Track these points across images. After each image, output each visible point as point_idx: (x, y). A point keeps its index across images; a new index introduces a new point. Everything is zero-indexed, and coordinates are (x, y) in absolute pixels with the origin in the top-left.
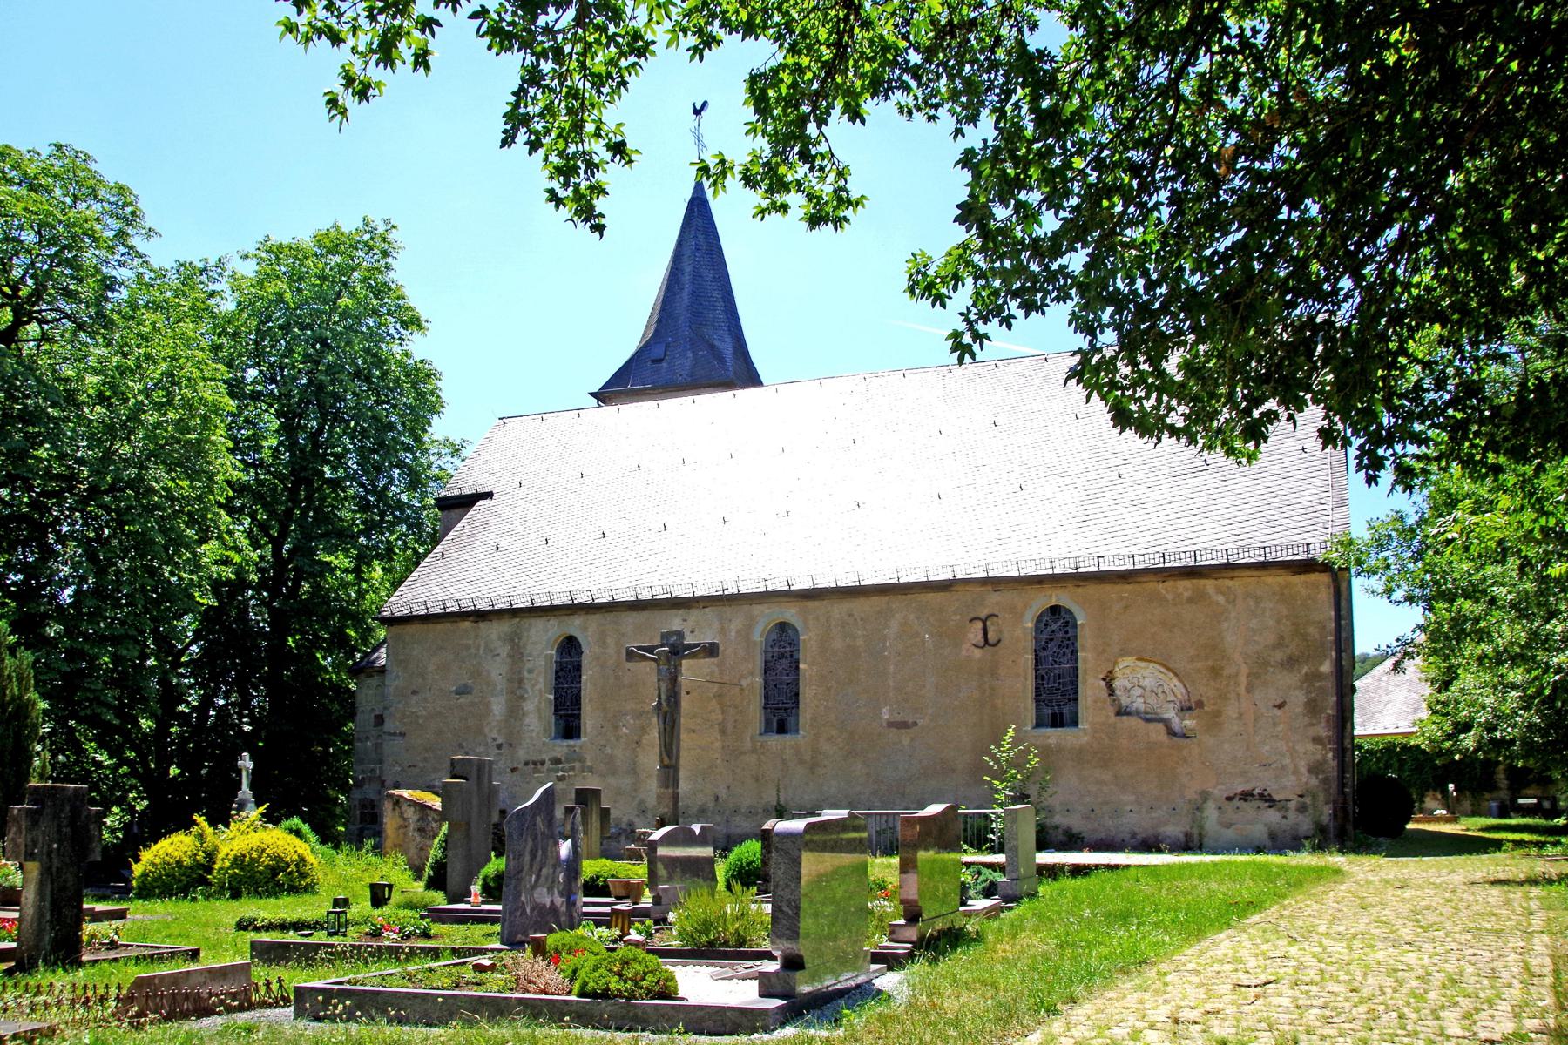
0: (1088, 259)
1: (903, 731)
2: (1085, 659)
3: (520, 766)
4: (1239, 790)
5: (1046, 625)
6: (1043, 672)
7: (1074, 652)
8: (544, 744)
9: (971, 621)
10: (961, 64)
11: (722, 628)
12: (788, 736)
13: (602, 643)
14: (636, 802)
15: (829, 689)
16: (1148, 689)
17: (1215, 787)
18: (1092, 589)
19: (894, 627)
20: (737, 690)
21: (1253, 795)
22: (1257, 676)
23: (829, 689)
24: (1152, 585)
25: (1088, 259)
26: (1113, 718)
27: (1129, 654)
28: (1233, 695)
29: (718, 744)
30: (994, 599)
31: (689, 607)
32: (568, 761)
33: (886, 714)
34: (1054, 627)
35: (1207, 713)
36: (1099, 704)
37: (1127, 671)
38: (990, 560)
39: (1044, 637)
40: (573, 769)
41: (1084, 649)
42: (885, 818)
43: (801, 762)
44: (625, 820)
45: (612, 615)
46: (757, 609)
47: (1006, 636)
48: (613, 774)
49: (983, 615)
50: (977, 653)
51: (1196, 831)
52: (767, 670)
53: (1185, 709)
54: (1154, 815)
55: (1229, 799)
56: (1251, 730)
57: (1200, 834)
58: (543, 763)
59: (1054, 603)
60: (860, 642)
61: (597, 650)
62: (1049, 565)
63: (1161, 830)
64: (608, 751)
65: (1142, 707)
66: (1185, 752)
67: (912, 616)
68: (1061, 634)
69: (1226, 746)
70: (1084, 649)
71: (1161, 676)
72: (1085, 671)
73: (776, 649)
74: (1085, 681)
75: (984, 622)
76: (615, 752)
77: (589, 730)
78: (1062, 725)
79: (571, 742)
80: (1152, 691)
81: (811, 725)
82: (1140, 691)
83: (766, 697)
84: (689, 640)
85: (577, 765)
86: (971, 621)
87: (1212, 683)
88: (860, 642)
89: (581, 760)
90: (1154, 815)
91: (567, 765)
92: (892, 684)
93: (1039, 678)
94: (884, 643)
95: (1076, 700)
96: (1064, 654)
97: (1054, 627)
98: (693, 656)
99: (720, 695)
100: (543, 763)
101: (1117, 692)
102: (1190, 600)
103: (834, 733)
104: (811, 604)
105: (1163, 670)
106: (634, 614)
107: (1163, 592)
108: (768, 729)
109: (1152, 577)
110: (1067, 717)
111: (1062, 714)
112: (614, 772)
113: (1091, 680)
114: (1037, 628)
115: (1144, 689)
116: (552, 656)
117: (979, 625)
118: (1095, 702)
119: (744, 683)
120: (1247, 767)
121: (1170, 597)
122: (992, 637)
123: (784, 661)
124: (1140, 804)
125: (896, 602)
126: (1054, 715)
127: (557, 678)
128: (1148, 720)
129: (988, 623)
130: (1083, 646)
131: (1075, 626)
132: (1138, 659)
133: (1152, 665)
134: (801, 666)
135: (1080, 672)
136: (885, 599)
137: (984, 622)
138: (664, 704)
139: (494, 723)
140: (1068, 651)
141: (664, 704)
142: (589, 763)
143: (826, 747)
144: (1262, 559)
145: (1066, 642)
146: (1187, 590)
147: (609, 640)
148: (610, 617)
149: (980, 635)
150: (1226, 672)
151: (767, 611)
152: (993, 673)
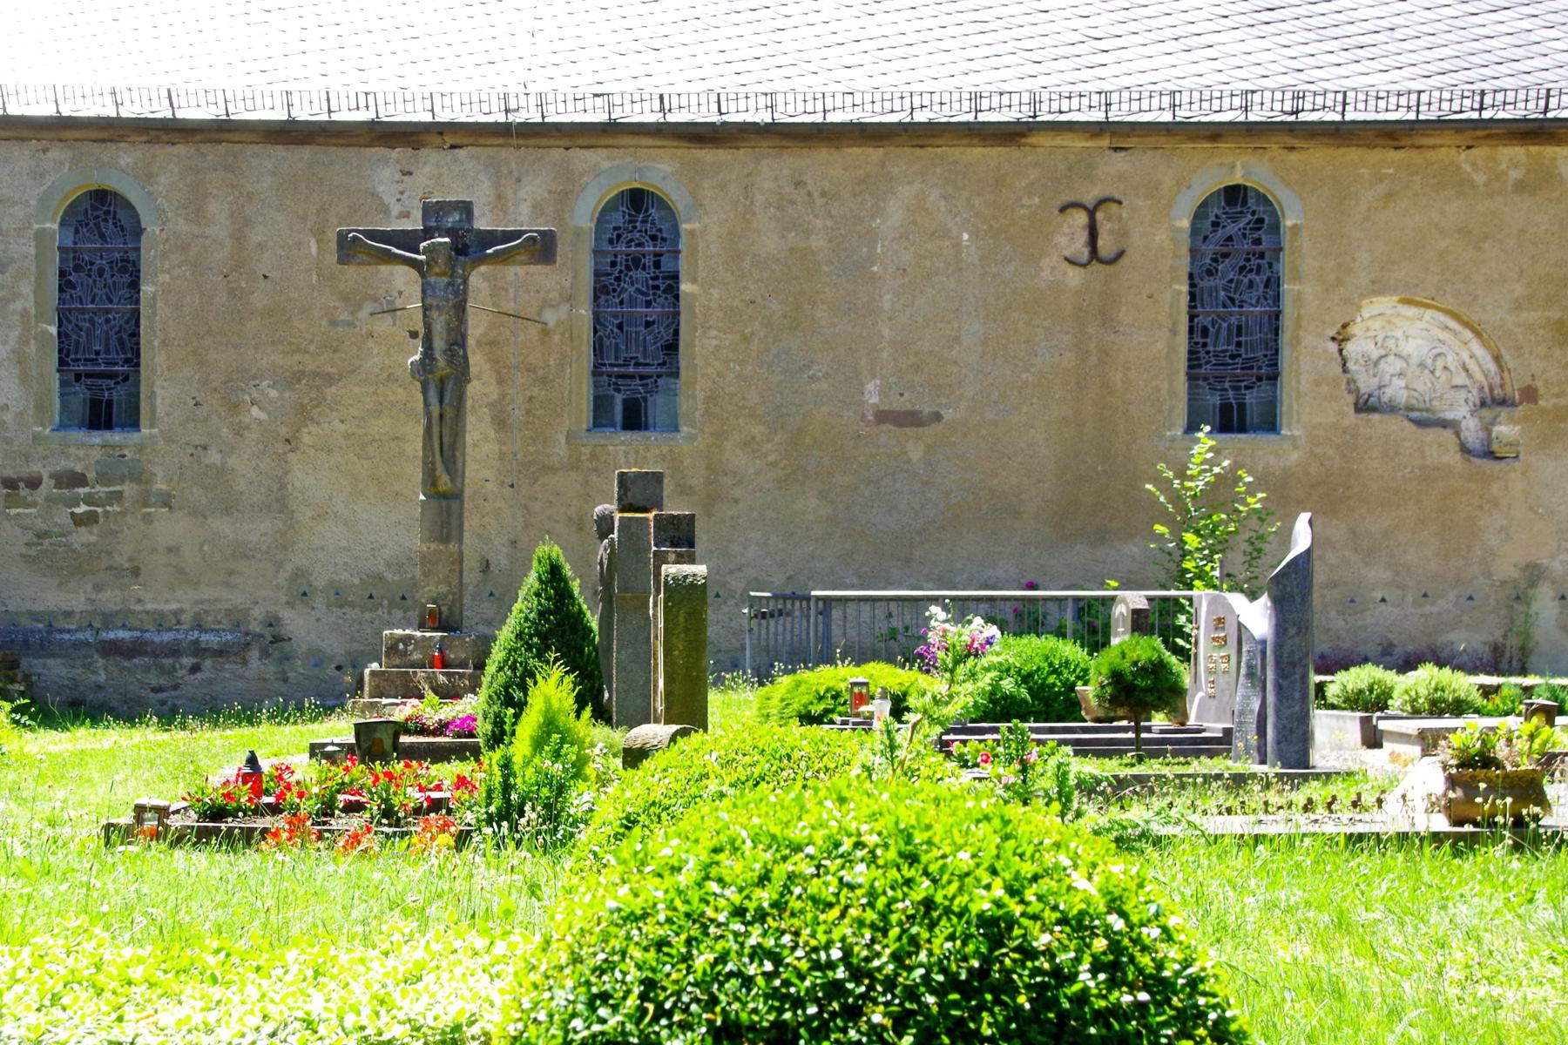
1: (909, 431)
2: (1299, 297)
6: (1207, 321)
7: (1273, 283)
8: (37, 438)
9: (1063, 210)
10: (1536, 513)
11: (499, 197)
12: (652, 436)
13: (195, 207)
14: (283, 575)
15: (747, 339)
18: (1318, 156)
19: (895, 213)
20: (534, 330)
23: (747, 339)
24: (1446, 153)
26: (1351, 418)
30: (1113, 171)
31: (417, 147)
32: (103, 479)
33: (872, 395)
34: (1232, 229)
35: (1544, 411)
36: (1324, 389)
37: (1376, 324)
38: (436, 89)
39: (1210, 249)
40: (118, 497)
41: (1297, 277)
42: (880, 610)
44: (258, 613)
45: (222, 149)
46: (583, 158)
47: (1136, 242)
48: (228, 511)
49: (1089, 199)
50: (1074, 276)
52: (601, 291)
53: (1493, 402)
54: (1428, 609)
58: (34, 483)
59: (1237, 179)
60: (818, 243)
61: (183, 227)
62: (108, 99)
64: (214, 457)
65: (1402, 397)
66: (1495, 489)
67: (934, 194)
68: (1247, 246)
70: (1297, 277)
71: (1444, 335)
73: (622, 247)
74: (1297, 341)
75: (1092, 214)
76: (233, 462)
77: (161, 409)
78: (1242, 429)
79: (115, 437)
80: (1422, 365)
81: (707, 413)
82: (1399, 365)
83: (599, 349)
84: (482, 223)
85: (129, 489)
86: (1063, 210)
87: (1558, 353)
88: (818, 243)
89: (139, 476)
90: (1428, 609)
91: (101, 490)
92: (886, 332)
93: (1197, 331)
94: (872, 248)
95: (1274, 378)
96: (1251, 284)
97: (1232, 229)
98: (504, 258)
99: (492, 343)
100: (34, 483)
102: (1520, 187)
103: (757, 430)
104: (707, 155)
105: (1453, 324)
106: (279, 151)
107: (1467, 167)
108: (601, 416)
109: (1450, 138)
110: (1253, 414)
111: (1242, 406)
112: (229, 507)
113: (1309, 340)
114: (1194, 231)
115: (1406, 359)
116: (52, 233)
117: (1081, 218)
118: (1317, 384)
119: (550, 317)
121: (1480, 179)
122: (1106, 245)
123: (638, 274)
124: (1403, 587)
125: (901, 160)
126: (1225, 409)
127: (65, 285)
128: (1420, 423)
129: (1099, 216)
131: (1276, 228)
133: (1429, 313)
136: (874, 154)
138: (441, 360)
140: (1259, 280)
141: (441, 360)
142: (160, 486)
143: (738, 459)
144: (1412, 116)
145: (1254, 262)
146: (1516, 166)
147: (213, 207)
148: (214, 153)
149: (1082, 237)
151: (606, 165)
152: (1106, 319)
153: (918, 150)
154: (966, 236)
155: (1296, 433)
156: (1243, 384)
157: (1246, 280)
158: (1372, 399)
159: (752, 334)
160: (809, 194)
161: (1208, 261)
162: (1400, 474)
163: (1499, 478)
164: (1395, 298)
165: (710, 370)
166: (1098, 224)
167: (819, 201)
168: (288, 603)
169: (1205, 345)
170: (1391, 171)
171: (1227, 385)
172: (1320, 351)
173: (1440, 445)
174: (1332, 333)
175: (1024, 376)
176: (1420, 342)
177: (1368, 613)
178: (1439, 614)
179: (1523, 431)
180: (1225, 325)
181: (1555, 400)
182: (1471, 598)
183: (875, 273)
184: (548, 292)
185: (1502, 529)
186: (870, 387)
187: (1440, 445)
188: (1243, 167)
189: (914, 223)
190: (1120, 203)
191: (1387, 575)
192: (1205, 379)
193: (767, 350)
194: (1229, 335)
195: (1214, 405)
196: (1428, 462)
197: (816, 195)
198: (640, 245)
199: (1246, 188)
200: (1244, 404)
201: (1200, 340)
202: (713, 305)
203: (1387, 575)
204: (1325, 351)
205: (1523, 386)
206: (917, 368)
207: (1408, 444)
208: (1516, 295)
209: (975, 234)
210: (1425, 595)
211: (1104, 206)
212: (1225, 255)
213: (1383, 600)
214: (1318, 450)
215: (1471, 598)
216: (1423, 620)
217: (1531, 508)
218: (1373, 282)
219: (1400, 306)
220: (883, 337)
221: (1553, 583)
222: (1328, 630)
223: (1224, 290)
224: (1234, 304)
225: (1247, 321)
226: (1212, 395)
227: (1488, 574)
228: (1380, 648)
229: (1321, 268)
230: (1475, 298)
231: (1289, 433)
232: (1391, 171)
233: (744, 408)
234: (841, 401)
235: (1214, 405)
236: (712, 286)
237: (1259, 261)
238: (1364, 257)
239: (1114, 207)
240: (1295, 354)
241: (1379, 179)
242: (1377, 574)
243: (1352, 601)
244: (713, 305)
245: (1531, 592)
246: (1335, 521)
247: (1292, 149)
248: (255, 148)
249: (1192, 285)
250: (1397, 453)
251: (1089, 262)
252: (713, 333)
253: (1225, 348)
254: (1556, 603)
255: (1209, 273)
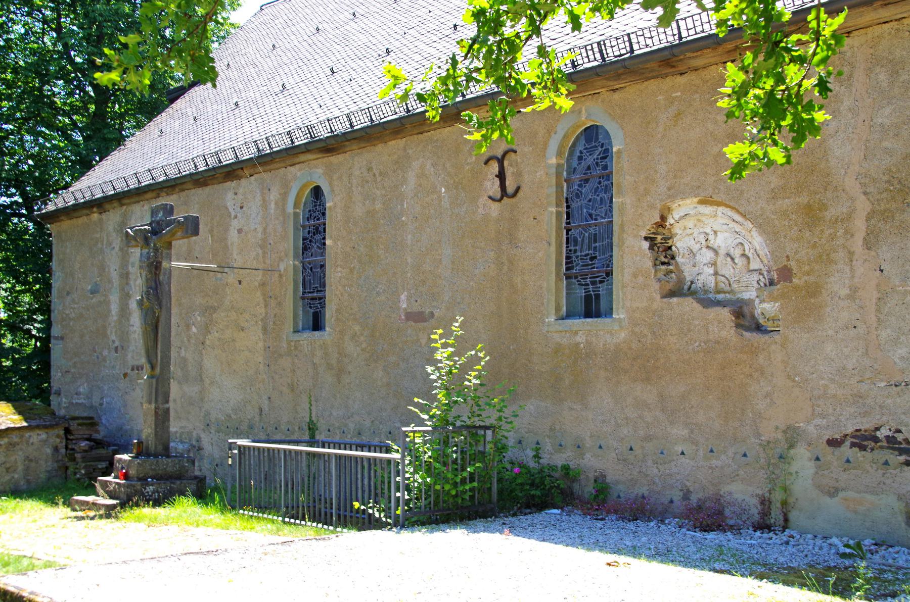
0: (737, 142)
3: (129, 371)
4: (850, 430)
5: (580, 158)
10: (794, 381)
11: (264, 200)
15: (352, 271)
16: (722, 252)
17: (808, 422)
21: (876, 440)
22: (886, 216)
25: (737, 142)
26: (659, 303)
27: (684, 196)
28: (841, 254)
29: (261, 344)
35: (796, 288)
36: (641, 279)
39: (576, 177)
43: (329, 367)
47: (526, 179)
50: (495, 206)
51: (777, 497)
54: (714, 462)
55: (833, 443)
56: (872, 319)
57: (784, 503)
63: (725, 489)
66: (761, 359)
69: (829, 348)
72: (622, 227)
75: (501, 161)
80: (728, 255)
88: (378, 206)
90: (714, 462)
92: (409, 260)
101: (679, 259)
113: (630, 241)
118: (635, 276)
120: (864, 387)
122: (510, 187)
124: (695, 443)
129: (506, 163)
130: (619, 185)
132: (701, 202)
133: (721, 209)
134: (328, 242)
135: (616, 228)
137: (501, 161)
139: (113, 324)
143: (351, 348)
150: (830, 214)
153: (420, 136)
154: (443, 190)
155: (622, 316)
156: (598, 279)
157: (599, 198)
158: (693, 286)
159: (354, 267)
160: (374, 175)
161: (576, 187)
162: (691, 347)
163: (763, 350)
164: (696, 200)
165: (338, 293)
166: (506, 170)
167: (379, 179)
168: (203, 430)
169: (575, 251)
170: (679, 94)
171: (588, 281)
172: (636, 249)
173: (720, 322)
174: (644, 234)
175: (471, 283)
176: (726, 235)
177: (673, 463)
178: (722, 467)
179: (782, 307)
180: (587, 235)
181: (806, 278)
182: (745, 455)
183: (403, 221)
184: (281, 252)
185: (767, 395)
186: (403, 297)
187: (720, 322)
188: (586, 110)
189: (420, 185)
190: (515, 152)
191: (685, 432)
192: (576, 277)
193: (360, 277)
194: (589, 242)
195: (581, 296)
196: (711, 337)
197: (377, 175)
198: (318, 219)
199: (597, 126)
200: (599, 295)
201: (573, 248)
202: (339, 252)
203: (685, 432)
204: (640, 248)
205: (781, 266)
206: (423, 282)
207: (697, 322)
208: (772, 186)
209: (447, 188)
210: (712, 451)
211: (507, 156)
212: (587, 181)
213: (683, 453)
214: (637, 329)
215: (745, 455)
216: (710, 471)
217: (789, 377)
218: (669, 189)
219: (699, 206)
220: (408, 263)
221: (810, 444)
222: (647, 476)
223: (586, 208)
224: (592, 218)
225: (600, 231)
226: (580, 289)
227: (758, 435)
228: (681, 494)
229: (635, 181)
230: (742, 193)
231: (617, 317)
232: (679, 94)
233: (352, 314)
234: (391, 307)
235: (581, 296)
236: (338, 240)
237: (606, 183)
238: (662, 168)
239: (513, 154)
240: (621, 253)
241: (671, 101)
242: (679, 431)
243: (662, 453)
244: (339, 252)
245: (792, 451)
246: (649, 387)
247: (614, 90)
248: (193, 191)
249: (568, 207)
250: (689, 330)
251: (502, 198)
252: (339, 269)
253: (587, 252)
254: (812, 464)
255: (577, 196)
